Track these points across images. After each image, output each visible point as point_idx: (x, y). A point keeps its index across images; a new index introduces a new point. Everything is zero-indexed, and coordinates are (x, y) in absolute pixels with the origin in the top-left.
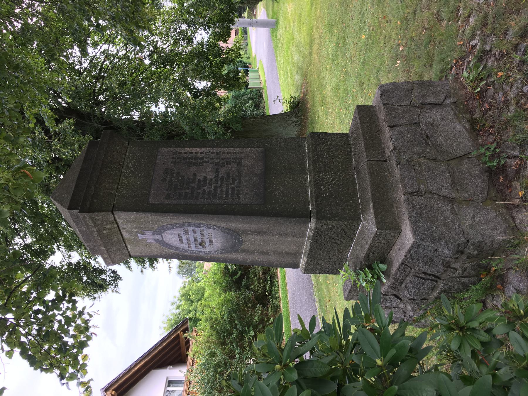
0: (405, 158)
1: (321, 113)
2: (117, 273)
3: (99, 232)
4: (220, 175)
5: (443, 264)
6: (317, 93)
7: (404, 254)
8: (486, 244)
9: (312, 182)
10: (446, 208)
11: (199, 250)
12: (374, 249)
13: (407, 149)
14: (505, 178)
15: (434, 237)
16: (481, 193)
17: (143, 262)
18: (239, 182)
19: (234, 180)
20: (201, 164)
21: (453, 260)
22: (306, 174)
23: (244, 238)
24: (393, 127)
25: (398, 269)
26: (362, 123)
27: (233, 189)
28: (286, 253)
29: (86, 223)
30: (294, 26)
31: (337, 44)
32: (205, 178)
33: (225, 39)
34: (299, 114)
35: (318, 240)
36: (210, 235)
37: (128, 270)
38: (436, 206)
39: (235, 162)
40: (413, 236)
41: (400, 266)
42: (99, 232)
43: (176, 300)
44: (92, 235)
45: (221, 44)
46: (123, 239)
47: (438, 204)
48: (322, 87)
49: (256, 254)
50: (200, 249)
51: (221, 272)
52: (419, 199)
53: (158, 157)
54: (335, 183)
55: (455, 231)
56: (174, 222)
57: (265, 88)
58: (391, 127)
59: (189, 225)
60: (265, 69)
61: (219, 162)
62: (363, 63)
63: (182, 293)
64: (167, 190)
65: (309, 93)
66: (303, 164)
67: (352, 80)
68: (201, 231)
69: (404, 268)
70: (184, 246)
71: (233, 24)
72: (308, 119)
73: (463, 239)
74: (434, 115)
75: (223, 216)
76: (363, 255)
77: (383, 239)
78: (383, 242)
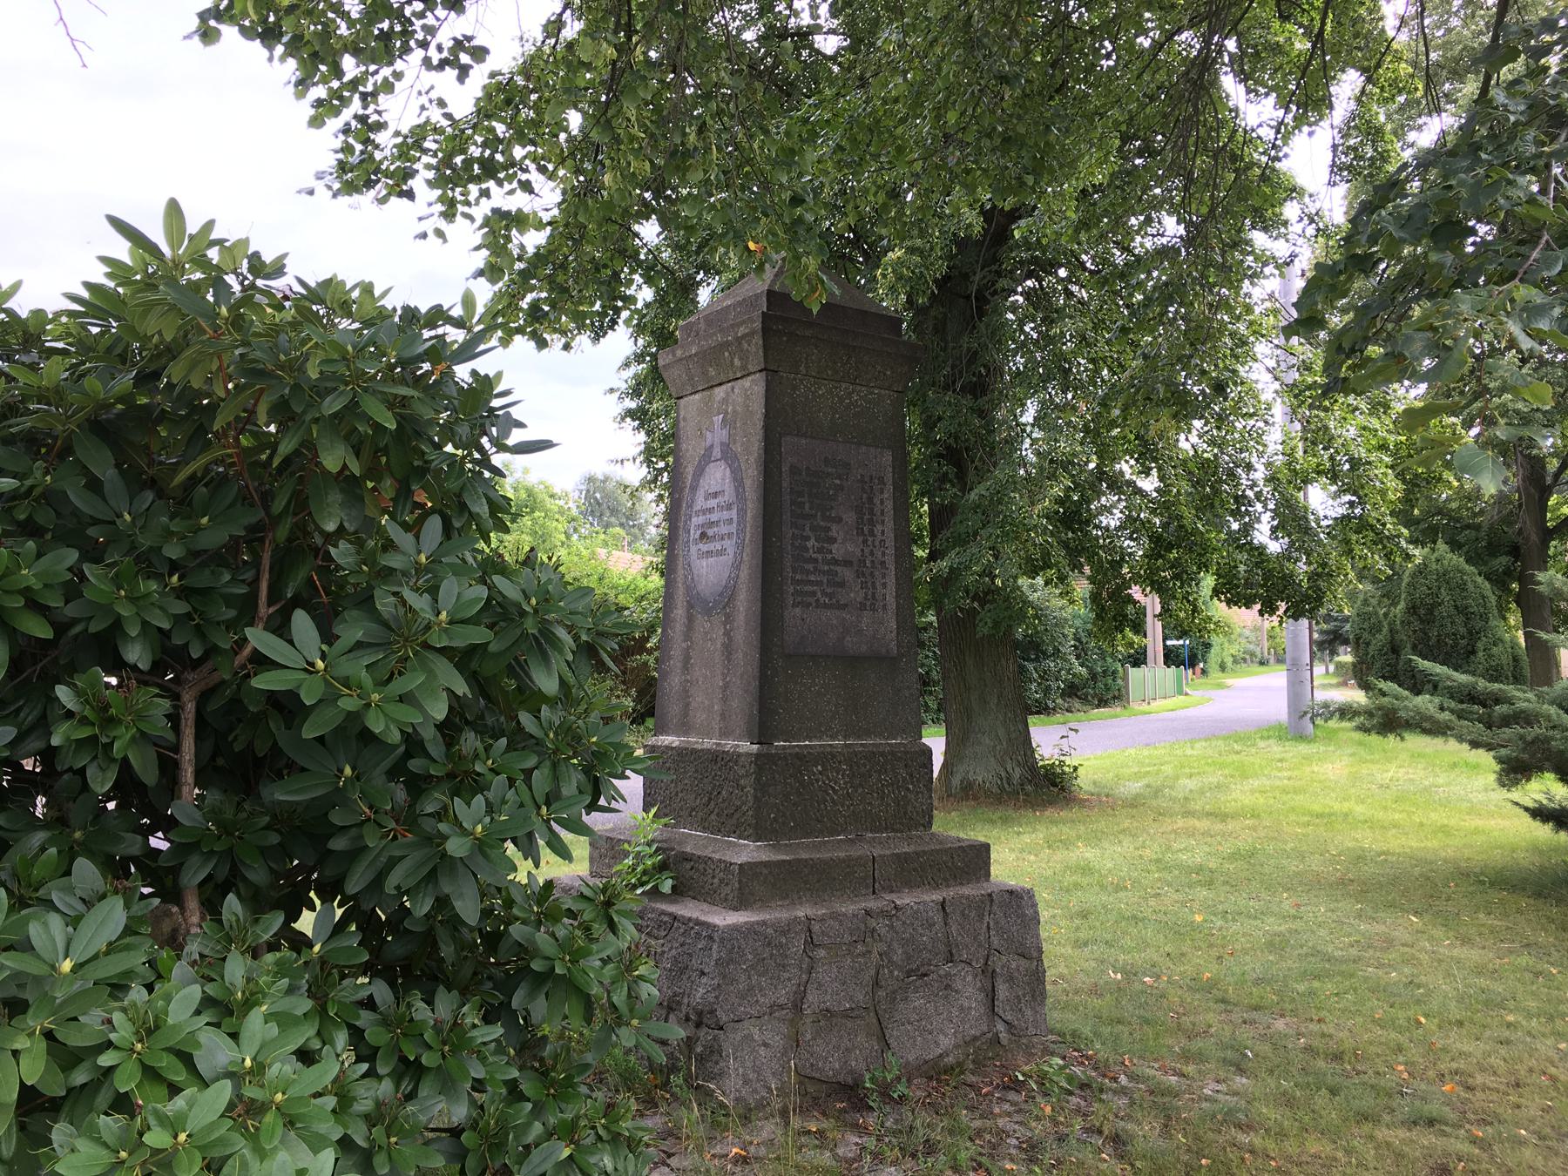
0: (881, 926)
1: (1027, 839)
2: (610, 332)
3: (725, 345)
4: (839, 569)
5: (675, 995)
6: (1082, 828)
7: (694, 916)
8: (717, 1063)
9: (818, 750)
10: (783, 995)
11: (692, 532)
12: (701, 867)
13: (897, 933)
14: (843, 1111)
15: (728, 964)
16: (812, 1065)
17: (635, 392)
18: (825, 606)
19: (831, 596)
20: (861, 532)
21: (682, 1015)
22: (846, 737)
23: (718, 619)
24: (943, 908)
25: (663, 913)
26: (950, 852)
27: (814, 594)
28: (688, 704)
29: (743, 322)
30: (1280, 778)
31: (1199, 869)
32: (833, 540)
33: (1223, 593)
34: (1029, 788)
35: (716, 763)
36: (721, 552)
37: (620, 360)
38: (786, 975)
39: (866, 598)
40: (729, 925)
41: (670, 914)
42: (726, 345)
43: (518, 475)
44: (720, 331)
45: (1208, 581)
46: (712, 387)
47: (789, 979)
48: (1095, 839)
49: (684, 645)
50: (695, 534)
51: (606, 594)
52: (798, 945)
53: (872, 450)
54: (828, 794)
55: (740, 1005)
56: (748, 483)
57: (1126, 713)
58: (943, 904)
59: (742, 512)
60: (1190, 712)
61: (865, 566)
62: (1134, 917)
63: (539, 489)
64: (808, 468)
65: (1085, 812)
66: (868, 733)
67: (1094, 899)
68: (730, 535)
69: (665, 923)
70: (700, 503)
71: (1261, 613)
72: (1016, 808)
73: (725, 1019)
74: (969, 992)
75: (760, 576)
76: (688, 850)
77: (721, 881)
78: (716, 881)
